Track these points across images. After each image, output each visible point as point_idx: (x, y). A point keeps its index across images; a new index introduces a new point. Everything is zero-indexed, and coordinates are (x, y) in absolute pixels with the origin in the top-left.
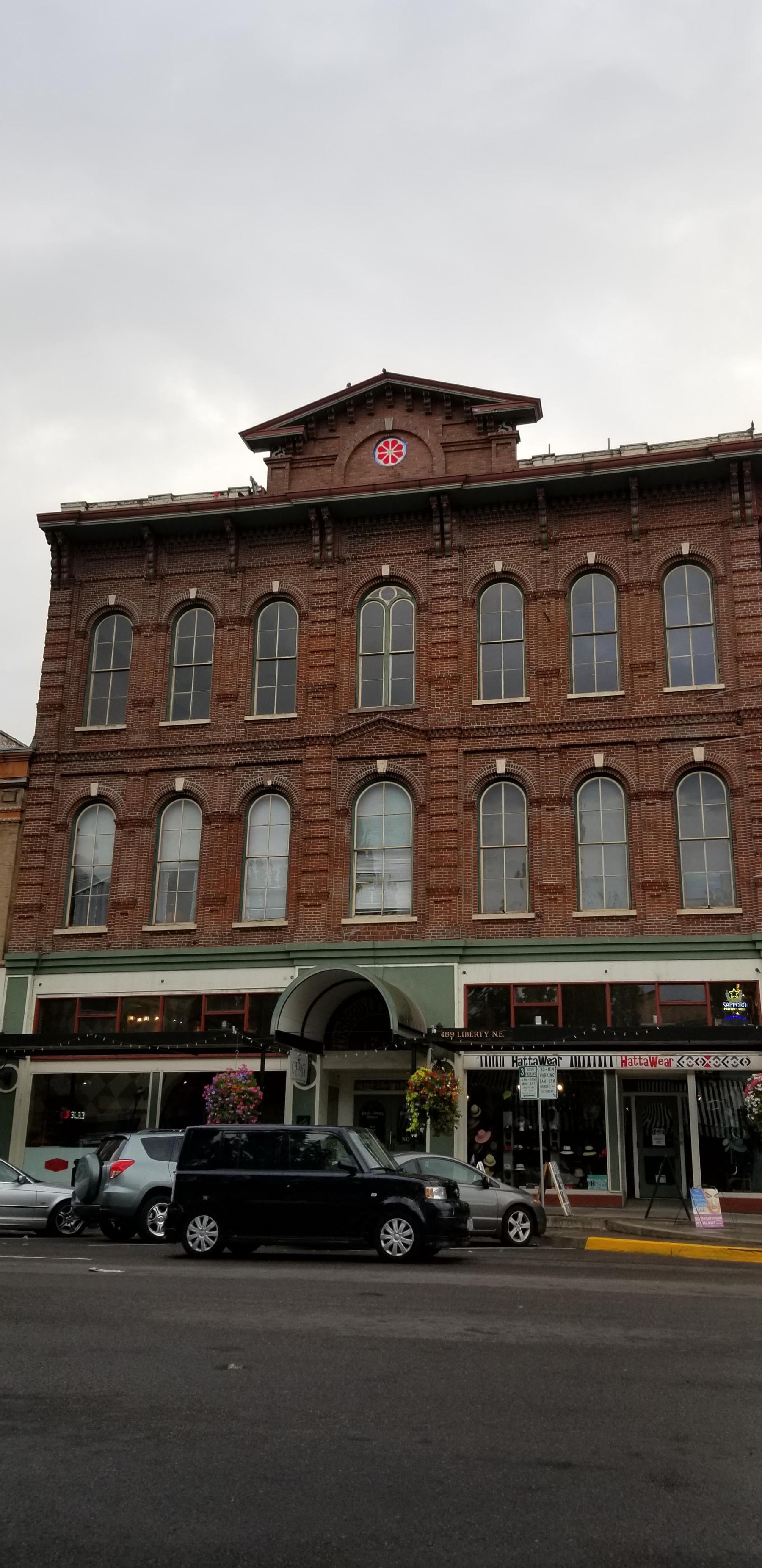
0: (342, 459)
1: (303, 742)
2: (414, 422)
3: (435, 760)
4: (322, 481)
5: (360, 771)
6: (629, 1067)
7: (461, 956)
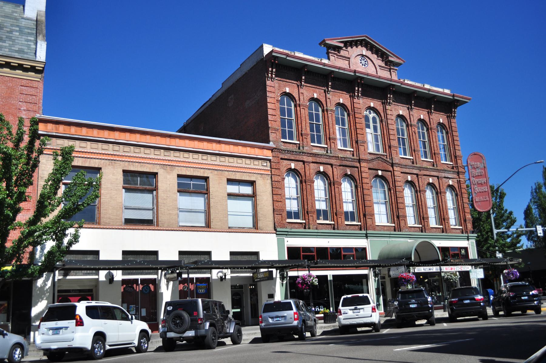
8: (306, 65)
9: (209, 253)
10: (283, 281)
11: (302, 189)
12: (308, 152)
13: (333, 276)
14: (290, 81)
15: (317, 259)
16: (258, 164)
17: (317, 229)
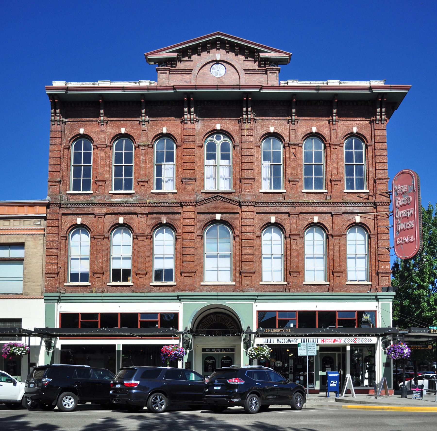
0: (195, 72)
1: (181, 205)
2: (230, 57)
3: (244, 215)
4: (185, 81)
5: (264, 219)
6: (324, 343)
7: (256, 299)
8: (294, 94)
9: (19, 321)
10: (49, 350)
11: (328, 246)
12: (100, 202)
13: (123, 345)
14: (88, 119)
15: (101, 327)
16: (30, 224)
17: (340, 291)
